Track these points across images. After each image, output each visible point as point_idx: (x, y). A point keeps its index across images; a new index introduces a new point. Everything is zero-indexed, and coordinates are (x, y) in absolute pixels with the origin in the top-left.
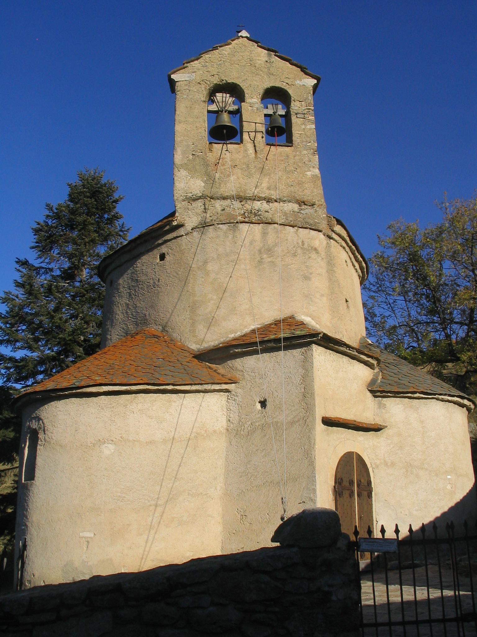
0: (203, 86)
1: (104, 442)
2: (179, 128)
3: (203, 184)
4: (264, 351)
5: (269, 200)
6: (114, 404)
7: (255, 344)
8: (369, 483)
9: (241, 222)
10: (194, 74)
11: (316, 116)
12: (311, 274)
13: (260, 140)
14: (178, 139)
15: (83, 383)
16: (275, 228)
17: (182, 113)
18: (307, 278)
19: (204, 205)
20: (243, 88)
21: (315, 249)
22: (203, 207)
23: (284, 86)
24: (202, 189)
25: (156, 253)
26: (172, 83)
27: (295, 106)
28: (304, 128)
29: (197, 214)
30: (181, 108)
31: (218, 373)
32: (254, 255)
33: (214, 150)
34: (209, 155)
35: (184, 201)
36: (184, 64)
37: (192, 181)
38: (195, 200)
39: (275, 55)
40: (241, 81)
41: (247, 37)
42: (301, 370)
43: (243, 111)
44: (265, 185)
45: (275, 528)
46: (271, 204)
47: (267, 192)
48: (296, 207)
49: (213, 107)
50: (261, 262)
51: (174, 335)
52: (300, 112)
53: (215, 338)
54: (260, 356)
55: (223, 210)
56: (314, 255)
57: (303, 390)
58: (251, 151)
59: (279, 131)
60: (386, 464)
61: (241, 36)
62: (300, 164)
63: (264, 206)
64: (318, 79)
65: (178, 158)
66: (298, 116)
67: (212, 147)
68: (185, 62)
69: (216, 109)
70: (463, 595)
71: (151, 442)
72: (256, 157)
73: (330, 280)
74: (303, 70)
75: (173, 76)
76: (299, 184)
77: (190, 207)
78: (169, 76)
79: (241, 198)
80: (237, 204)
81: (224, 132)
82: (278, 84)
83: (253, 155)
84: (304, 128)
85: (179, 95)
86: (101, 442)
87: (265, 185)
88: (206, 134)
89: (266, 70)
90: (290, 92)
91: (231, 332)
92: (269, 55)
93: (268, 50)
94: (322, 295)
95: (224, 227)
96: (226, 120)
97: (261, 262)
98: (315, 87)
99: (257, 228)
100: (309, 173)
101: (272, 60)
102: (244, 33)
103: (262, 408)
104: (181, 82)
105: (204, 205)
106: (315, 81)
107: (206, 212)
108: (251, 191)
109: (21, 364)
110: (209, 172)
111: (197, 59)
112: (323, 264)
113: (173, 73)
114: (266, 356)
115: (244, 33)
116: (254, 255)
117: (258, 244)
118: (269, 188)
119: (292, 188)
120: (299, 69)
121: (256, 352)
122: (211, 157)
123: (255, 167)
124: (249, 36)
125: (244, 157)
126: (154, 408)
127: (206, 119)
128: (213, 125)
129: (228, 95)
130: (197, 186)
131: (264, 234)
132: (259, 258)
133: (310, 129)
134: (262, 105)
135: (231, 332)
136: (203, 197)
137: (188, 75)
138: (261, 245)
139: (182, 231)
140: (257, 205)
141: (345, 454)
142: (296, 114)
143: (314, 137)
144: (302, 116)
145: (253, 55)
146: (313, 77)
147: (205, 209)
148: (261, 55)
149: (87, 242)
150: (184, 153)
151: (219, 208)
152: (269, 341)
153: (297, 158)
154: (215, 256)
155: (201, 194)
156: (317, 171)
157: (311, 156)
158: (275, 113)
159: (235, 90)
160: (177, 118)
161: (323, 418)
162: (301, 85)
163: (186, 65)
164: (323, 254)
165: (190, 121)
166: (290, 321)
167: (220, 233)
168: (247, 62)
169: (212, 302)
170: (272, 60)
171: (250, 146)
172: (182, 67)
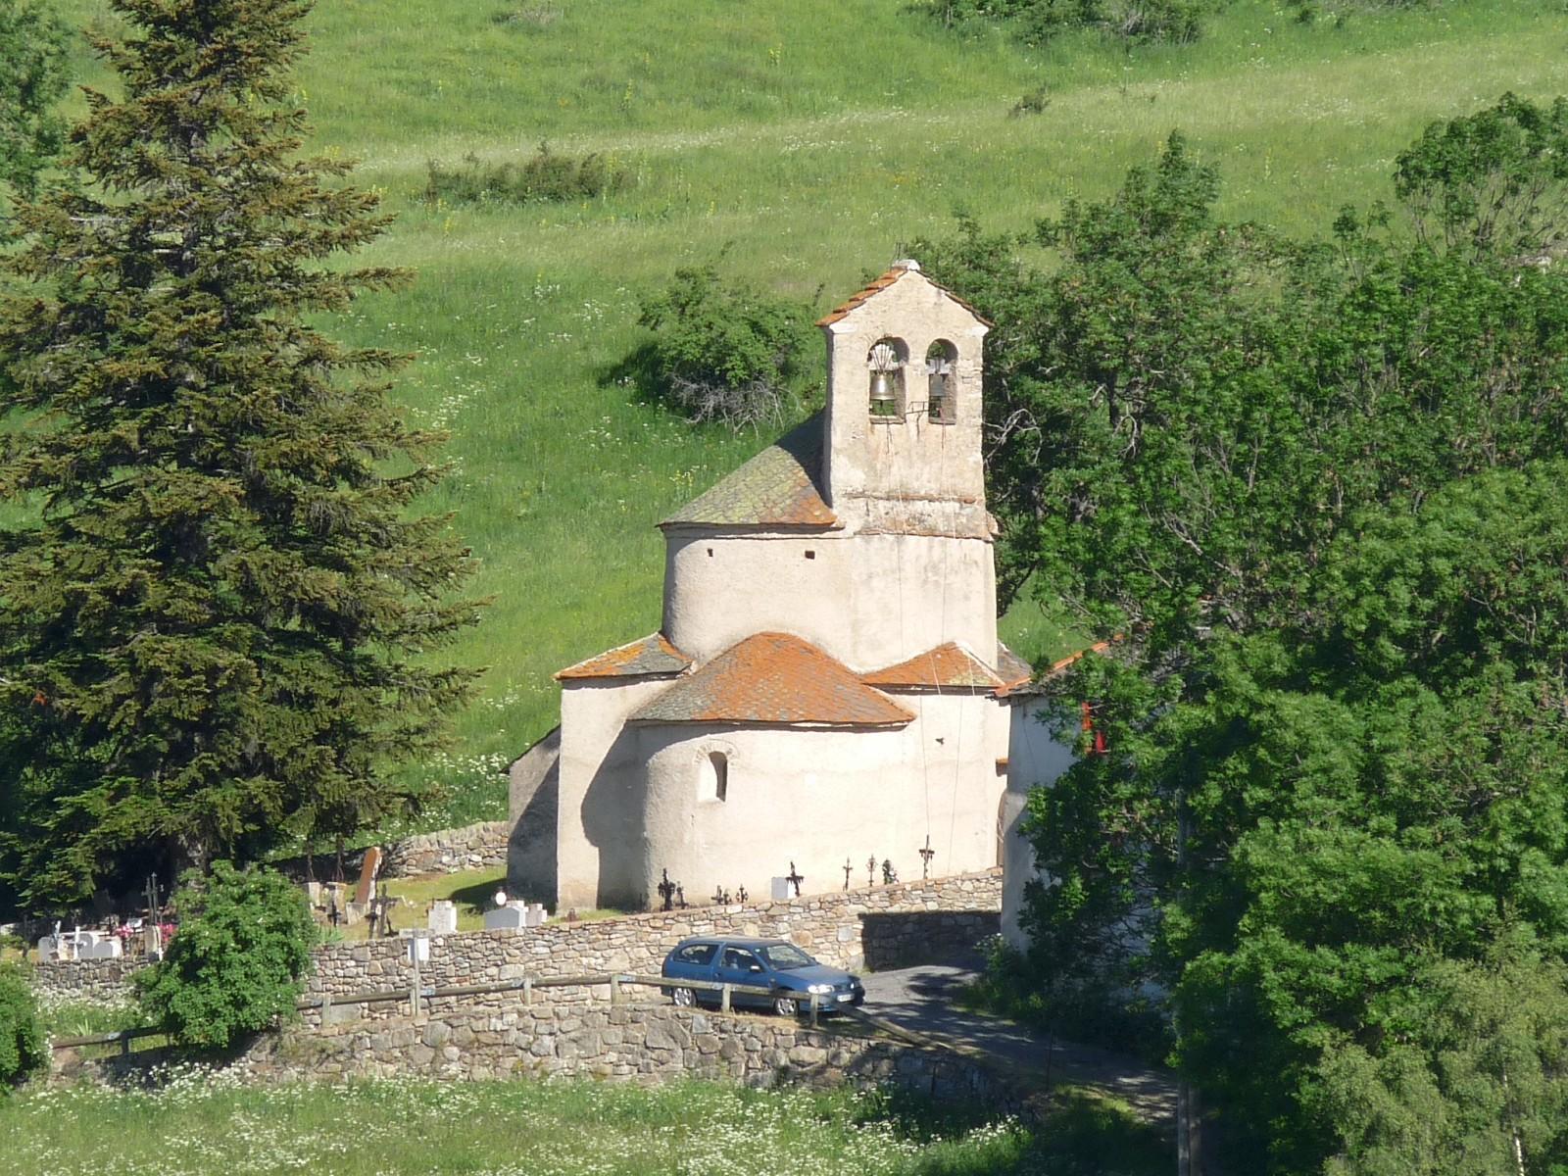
18: (967, 598)
28: (969, 397)
29: (860, 517)
34: (870, 437)
44: (925, 477)
45: (579, 813)
59: (938, 407)
72: (918, 440)
80: (901, 505)
81: (885, 408)
87: (925, 477)
89: (933, 316)
90: (958, 347)
95: (891, 538)
97: (925, 582)
103: (1355, 885)
109: (272, 657)
110: (869, 460)
117: (924, 561)
122: (873, 440)
136: (862, 495)
139: (839, 534)
140: (919, 506)
149: (1355, 457)
151: (883, 512)
171: (912, 426)
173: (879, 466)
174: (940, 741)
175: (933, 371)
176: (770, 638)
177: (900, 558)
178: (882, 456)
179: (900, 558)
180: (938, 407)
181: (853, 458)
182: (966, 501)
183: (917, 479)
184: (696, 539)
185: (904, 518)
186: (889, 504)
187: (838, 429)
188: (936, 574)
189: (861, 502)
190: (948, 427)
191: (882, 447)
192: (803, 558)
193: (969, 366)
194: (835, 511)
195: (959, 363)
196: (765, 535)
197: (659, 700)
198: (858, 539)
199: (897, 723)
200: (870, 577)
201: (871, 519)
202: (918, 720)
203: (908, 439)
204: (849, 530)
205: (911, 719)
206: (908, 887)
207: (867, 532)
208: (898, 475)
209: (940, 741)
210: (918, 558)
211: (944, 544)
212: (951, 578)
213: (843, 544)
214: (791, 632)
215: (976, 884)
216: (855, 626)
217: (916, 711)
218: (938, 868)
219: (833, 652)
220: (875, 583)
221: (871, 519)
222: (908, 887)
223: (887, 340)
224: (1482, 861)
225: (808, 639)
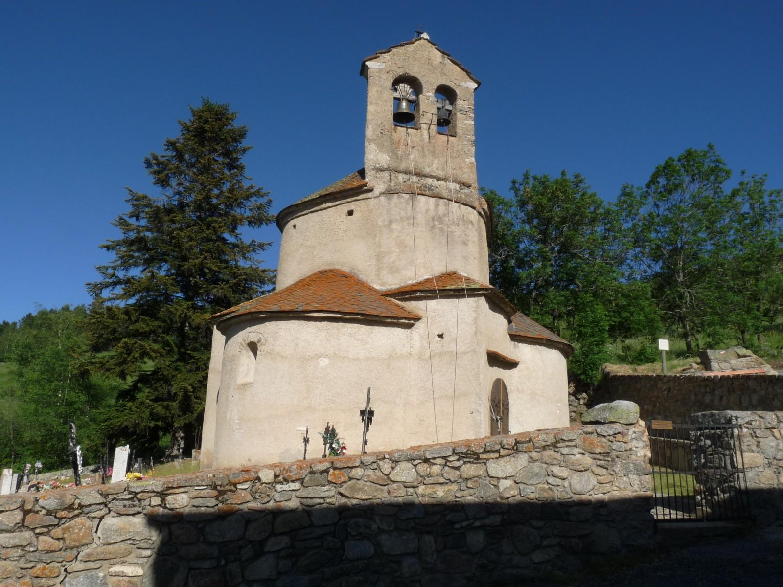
0: (391, 76)
1: (321, 356)
2: (370, 108)
3: (388, 159)
4: (442, 297)
5: (438, 179)
6: (329, 327)
7: (434, 291)
8: (508, 404)
9: (419, 194)
10: (384, 64)
11: (475, 114)
12: (468, 240)
13: (434, 128)
14: (369, 117)
15: (309, 308)
16: (444, 202)
17: (373, 95)
18: (465, 243)
19: (390, 176)
20: (422, 82)
21: (472, 222)
22: (388, 177)
23: (452, 85)
24: (388, 163)
25: (346, 208)
26: (364, 71)
27: (460, 103)
28: (465, 122)
29: (384, 183)
30: (373, 92)
31: (405, 311)
32: (429, 221)
33: (398, 131)
35: (373, 170)
36: (377, 54)
37: (380, 155)
38: (382, 170)
39: (448, 59)
40: (420, 75)
41: (427, 39)
42: (474, 315)
43: (421, 102)
44: (435, 166)
46: (439, 182)
47: (437, 171)
48: (457, 186)
49: (397, 95)
50: (433, 227)
51: (361, 276)
52: (463, 109)
53: (396, 282)
54: (439, 300)
55: (405, 182)
56: (470, 226)
57: (474, 329)
58: (426, 136)
59: (445, 122)
60: (518, 390)
61: (423, 38)
62: (462, 152)
63: (435, 183)
64: (479, 85)
65: (369, 132)
66: (462, 112)
67: (397, 129)
68: (379, 52)
69: (399, 97)
70: (667, 441)
71: (357, 359)
72: (429, 142)
73: (480, 246)
74: (468, 73)
75: (369, 64)
76: (460, 168)
77: (378, 175)
78: (364, 62)
79: (418, 174)
80: (415, 179)
81: (403, 118)
82: (448, 83)
83: (427, 140)
84: (465, 122)
85: (370, 80)
86: (318, 356)
88: (391, 117)
89: (440, 70)
90: (457, 91)
91: (410, 279)
92: (443, 58)
93: (443, 53)
94: (475, 258)
95: (407, 196)
96: (404, 107)
97: (433, 227)
98: (475, 89)
99: (432, 200)
100: (468, 161)
101: (446, 62)
102: (425, 35)
104: (374, 70)
105: (390, 176)
106: (476, 85)
107: (391, 182)
108: (427, 170)
111: (388, 52)
112: (476, 234)
113: (368, 60)
114: (444, 301)
115: (425, 35)
116: (429, 221)
117: (432, 213)
118: (437, 169)
119: (455, 171)
120: (465, 73)
121: (435, 298)
122: (396, 136)
123: (428, 150)
124: (429, 38)
125: (421, 141)
126: (360, 333)
127: (393, 105)
128: (396, 111)
129: (409, 86)
130: (384, 159)
131: (437, 206)
132: (432, 224)
133: (470, 125)
134: (435, 99)
135: (410, 279)
136: (388, 169)
137: (379, 64)
138: (434, 214)
139: (370, 195)
140: (430, 181)
141: (494, 382)
142: (461, 110)
143: (472, 132)
144: (465, 113)
145: (431, 55)
146: (476, 81)
147: (390, 179)
148: (437, 56)
150: (374, 130)
152: (450, 290)
153: (460, 147)
154: (399, 218)
155: (386, 167)
156: (473, 159)
157: (470, 147)
158: (443, 107)
159: (415, 84)
160: (369, 100)
161: (488, 351)
162: (465, 86)
163: (378, 55)
164: (476, 225)
165: (379, 104)
166: (451, 275)
167: (403, 200)
168: (425, 59)
169: (395, 254)
170: (446, 62)
171: (425, 133)
172: (375, 56)
173: (400, 153)
174: (441, 336)
175: (440, 106)
176: (321, 272)
177: (414, 210)
178: (402, 147)
179: (414, 210)
180: (445, 122)
181: (381, 147)
182: (423, 76)
183: (429, 166)
184: (288, 221)
185: (416, 185)
186: (407, 177)
187: (370, 127)
188: (441, 223)
189: (386, 174)
190: (451, 139)
191: (402, 141)
192: (484, 359)
193: (465, 102)
194: (367, 180)
195: (458, 102)
196: (324, 206)
197: (142, 298)
198: (382, 198)
199: (409, 322)
200: (391, 222)
201: (392, 185)
202: (423, 320)
203: (422, 140)
204: (377, 192)
205: (417, 319)
206: (267, 476)
207: (390, 192)
208: (413, 160)
209: (441, 336)
210: (427, 211)
211: (447, 205)
212: (453, 228)
213: (372, 202)
214: (337, 267)
215: (423, 468)
216: (379, 257)
217: (421, 313)
218: (381, 439)
219: (363, 277)
220: (394, 226)
221: (392, 185)
222: (267, 476)
223: (397, 82)
224: (132, 436)
225: (346, 269)
